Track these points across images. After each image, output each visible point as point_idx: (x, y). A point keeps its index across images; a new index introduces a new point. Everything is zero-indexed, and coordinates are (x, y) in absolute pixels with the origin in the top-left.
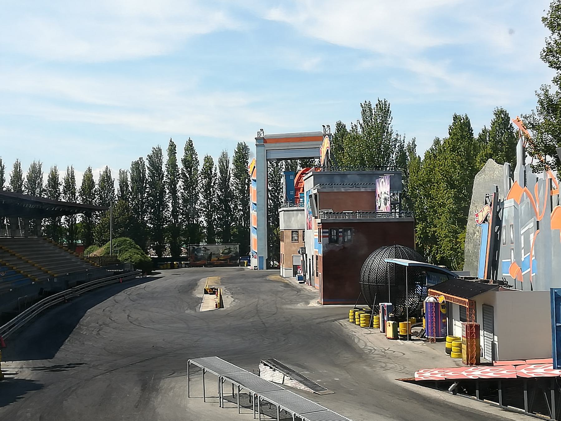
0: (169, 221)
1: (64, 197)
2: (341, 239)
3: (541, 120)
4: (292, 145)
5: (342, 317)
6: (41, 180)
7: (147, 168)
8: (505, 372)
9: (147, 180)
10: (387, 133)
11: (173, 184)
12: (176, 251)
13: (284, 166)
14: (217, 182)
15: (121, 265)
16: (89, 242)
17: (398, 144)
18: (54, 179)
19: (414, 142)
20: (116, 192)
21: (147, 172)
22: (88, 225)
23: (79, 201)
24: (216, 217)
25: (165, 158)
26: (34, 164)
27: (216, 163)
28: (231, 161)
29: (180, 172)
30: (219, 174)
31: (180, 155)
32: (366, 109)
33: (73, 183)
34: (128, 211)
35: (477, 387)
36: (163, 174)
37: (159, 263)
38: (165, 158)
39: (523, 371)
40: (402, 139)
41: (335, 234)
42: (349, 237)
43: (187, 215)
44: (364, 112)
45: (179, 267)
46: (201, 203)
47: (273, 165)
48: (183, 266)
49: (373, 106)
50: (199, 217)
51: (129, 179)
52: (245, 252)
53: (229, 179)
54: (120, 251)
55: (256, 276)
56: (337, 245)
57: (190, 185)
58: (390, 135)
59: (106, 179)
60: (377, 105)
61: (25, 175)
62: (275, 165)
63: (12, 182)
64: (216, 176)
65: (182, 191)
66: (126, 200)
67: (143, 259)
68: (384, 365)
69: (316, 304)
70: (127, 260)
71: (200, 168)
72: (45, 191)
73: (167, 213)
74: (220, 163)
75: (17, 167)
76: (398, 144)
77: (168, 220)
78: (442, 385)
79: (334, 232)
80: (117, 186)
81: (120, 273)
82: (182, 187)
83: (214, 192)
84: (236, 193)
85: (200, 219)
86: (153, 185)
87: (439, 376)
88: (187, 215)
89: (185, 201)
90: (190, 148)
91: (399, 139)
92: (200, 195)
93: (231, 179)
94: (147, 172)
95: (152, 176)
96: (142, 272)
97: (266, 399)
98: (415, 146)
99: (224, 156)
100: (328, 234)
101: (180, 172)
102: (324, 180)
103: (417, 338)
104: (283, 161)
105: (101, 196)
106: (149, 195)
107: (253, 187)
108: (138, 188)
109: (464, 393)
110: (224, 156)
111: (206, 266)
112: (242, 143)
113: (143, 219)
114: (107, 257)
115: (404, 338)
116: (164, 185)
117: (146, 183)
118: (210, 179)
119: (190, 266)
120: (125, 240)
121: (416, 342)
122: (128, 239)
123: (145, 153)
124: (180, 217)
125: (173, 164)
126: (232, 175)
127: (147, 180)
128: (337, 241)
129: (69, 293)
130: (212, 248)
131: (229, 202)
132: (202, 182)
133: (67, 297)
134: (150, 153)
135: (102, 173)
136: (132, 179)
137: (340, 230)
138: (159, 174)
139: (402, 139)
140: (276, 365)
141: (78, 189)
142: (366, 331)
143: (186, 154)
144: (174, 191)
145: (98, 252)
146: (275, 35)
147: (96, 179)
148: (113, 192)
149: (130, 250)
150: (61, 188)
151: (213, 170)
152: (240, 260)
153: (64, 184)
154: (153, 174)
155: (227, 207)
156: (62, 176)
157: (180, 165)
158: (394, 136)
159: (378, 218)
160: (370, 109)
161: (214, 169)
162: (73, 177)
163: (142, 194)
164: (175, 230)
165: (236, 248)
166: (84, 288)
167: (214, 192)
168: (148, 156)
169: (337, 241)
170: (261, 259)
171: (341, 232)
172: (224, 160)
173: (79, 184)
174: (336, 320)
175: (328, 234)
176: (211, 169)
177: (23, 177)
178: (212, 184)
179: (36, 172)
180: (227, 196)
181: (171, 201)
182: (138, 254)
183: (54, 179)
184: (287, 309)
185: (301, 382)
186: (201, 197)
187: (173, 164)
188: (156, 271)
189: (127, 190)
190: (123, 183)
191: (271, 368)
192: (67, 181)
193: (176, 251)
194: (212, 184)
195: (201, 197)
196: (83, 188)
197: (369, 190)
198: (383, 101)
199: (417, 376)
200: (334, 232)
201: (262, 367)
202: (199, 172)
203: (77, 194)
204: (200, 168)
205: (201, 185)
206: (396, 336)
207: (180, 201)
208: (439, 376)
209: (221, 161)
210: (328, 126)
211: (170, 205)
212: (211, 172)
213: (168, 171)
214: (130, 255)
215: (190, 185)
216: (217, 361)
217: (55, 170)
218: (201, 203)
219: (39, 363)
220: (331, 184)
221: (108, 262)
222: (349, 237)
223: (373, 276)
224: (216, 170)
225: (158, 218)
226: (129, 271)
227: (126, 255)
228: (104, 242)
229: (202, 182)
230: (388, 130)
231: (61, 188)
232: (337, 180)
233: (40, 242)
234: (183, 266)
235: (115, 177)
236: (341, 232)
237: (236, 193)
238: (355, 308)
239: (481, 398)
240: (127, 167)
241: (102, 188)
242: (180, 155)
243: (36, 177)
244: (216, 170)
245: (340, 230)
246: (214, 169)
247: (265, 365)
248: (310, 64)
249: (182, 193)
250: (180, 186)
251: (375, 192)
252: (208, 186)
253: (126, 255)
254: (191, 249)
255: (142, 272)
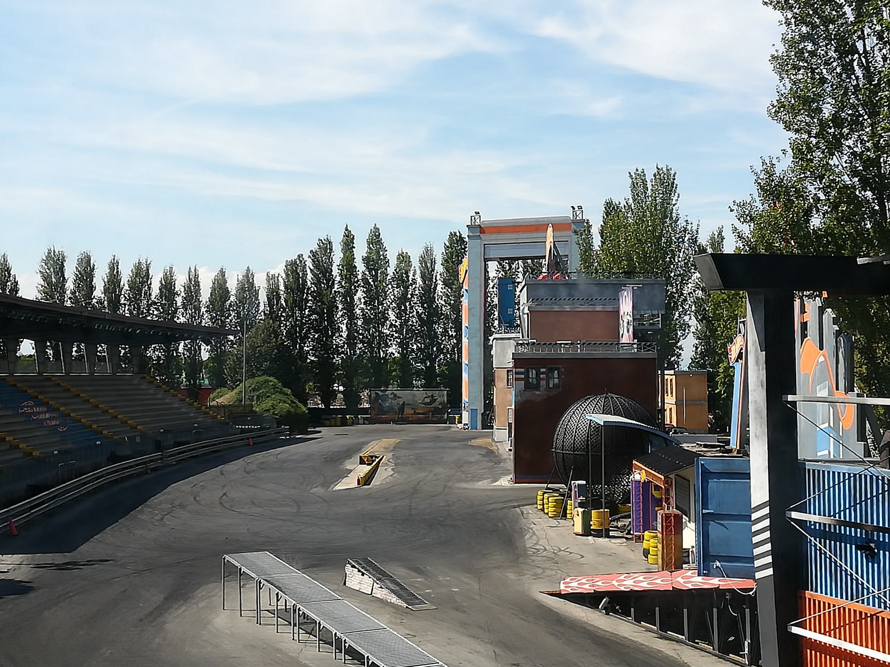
0: (343, 353)
1: (183, 314)
2: (543, 383)
3: (759, 206)
4: (523, 237)
5: (530, 501)
6: (149, 288)
7: (309, 271)
8: (659, 581)
9: (309, 289)
10: (671, 218)
11: (349, 294)
12: (352, 398)
13: (521, 269)
14: (417, 292)
15: (257, 418)
16: (220, 382)
17: (688, 237)
18: (168, 287)
19: (720, 233)
20: (262, 308)
21: (310, 276)
22: (218, 357)
23: (206, 321)
24: (415, 347)
25: (338, 256)
26: (140, 263)
27: (416, 263)
28: (439, 260)
29: (360, 277)
30: (419, 281)
31: (360, 251)
32: (638, 182)
33: (198, 292)
34: (276, 337)
35: (632, 604)
36: (334, 280)
37: (319, 418)
38: (338, 256)
39: (680, 579)
40: (694, 228)
41: (534, 376)
42: (556, 381)
43: (370, 343)
44: (634, 186)
45: (352, 424)
46: (391, 325)
47: (503, 267)
48: (361, 421)
49: (649, 177)
50: (387, 346)
51: (282, 287)
52: (455, 401)
53: (435, 288)
54: (258, 397)
55: (464, 440)
56: (538, 393)
57: (374, 296)
58: (676, 221)
59: (248, 286)
60: (655, 175)
61: (125, 280)
62: (508, 268)
63: (106, 291)
64: (415, 283)
65: (362, 306)
66: (277, 318)
67: (292, 410)
68: (539, 571)
69: (505, 482)
70: (268, 411)
71: (391, 271)
72: (155, 303)
73: (340, 340)
74: (421, 264)
75: (114, 267)
76: (688, 237)
77: (326, 352)
78: (621, 603)
79: (533, 373)
80: (263, 297)
81: (252, 430)
82: (363, 300)
83: (411, 308)
84: (446, 310)
85: (390, 350)
86: (319, 296)
87: (587, 586)
88: (370, 343)
89: (367, 321)
90: (375, 240)
91: (689, 227)
92: (390, 312)
93: (439, 288)
94: (310, 276)
95: (317, 283)
96: (290, 430)
97: (306, 611)
98: (723, 238)
99: (428, 251)
100: (523, 376)
101: (360, 277)
102: (542, 292)
103: (621, 534)
104: (520, 262)
105: (238, 313)
106: (312, 311)
107: (465, 301)
108: (294, 301)
109: (616, 612)
110: (428, 251)
111: (396, 422)
112: (455, 233)
113: (301, 348)
114: (238, 406)
115: (598, 534)
116: (334, 297)
117: (307, 294)
118: (407, 288)
119: (371, 421)
120: (267, 381)
121: (613, 541)
122: (271, 378)
123: (306, 248)
124: (360, 346)
125: (349, 265)
126: (439, 282)
127: (309, 289)
128: (537, 387)
129: (157, 460)
130: (405, 395)
131: (433, 322)
132: (393, 292)
133: (152, 465)
134: (315, 247)
135: (240, 278)
136: (286, 287)
137: (542, 370)
138: (328, 280)
139: (694, 228)
140: (368, 567)
141: (204, 302)
142: (554, 522)
143: (370, 248)
144: (350, 307)
145: (225, 398)
146: (548, 59)
147: (232, 285)
148: (258, 306)
149: (273, 396)
150: (179, 301)
151: (411, 275)
152: (449, 413)
153: (183, 294)
154: (318, 279)
155: (431, 330)
156: (180, 282)
157: (360, 267)
158: (681, 223)
159: (623, 353)
160: (644, 182)
161: (412, 272)
162: (197, 284)
163: (302, 310)
164: (352, 367)
165: (442, 395)
166: (185, 452)
167: (411, 308)
168: (311, 251)
169: (537, 387)
170: (473, 412)
171: (543, 373)
172: (427, 260)
173: (205, 295)
174: (519, 506)
175: (523, 376)
176: (407, 273)
177: (122, 283)
178: (409, 296)
179: (142, 275)
180: (432, 314)
181: (345, 322)
182: (285, 402)
183: (168, 287)
184: (459, 488)
185: (393, 591)
186: (392, 316)
187: (349, 265)
188: (317, 429)
189: (277, 304)
190: (273, 294)
191: (359, 571)
192: (188, 289)
193: (352, 398)
194: (409, 296)
195: (392, 316)
196: (212, 301)
197: (609, 308)
198: (665, 169)
199: (563, 588)
200: (533, 373)
201: (348, 569)
202: (389, 277)
203: (203, 310)
204: (391, 271)
205: (392, 297)
206: (587, 531)
207: (360, 323)
208: (587, 588)
209: (423, 260)
210: (580, 208)
211: (344, 327)
212: (408, 277)
213: (341, 275)
214: (275, 402)
215: (374, 296)
216: (266, 560)
217: (171, 272)
218: (391, 325)
219: (41, 558)
220: (555, 299)
221: (239, 413)
222: (556, 381)
223: (569, 440)
224: (416, 274)
225: (325, 348)
226: (269, 428)
227: (267, 404)
228: (236, 382)
229: (393, 292)
230: (671, 213)
231: (179, 301)
232: (563, 292)
233: (135, 382)
234: (361, 421)
235: (261, 282)
236: (543, 373)
237: (446, 310)
238: (547, 488)
239: (638, 620)
240: (279, 270)
241: (241, 300)
242: (360, 251)
243: (142, 283)
244: (416, 274)
245: (542, 370)
246: (412, 272)
247: (353, 566)
248: (603, 107)
249: (362, 309)
250: (360, 299)
251: (618, 312)
252: (403, 299)
253: (267, 404)
254: (373, 395)
255: (290, 430)
